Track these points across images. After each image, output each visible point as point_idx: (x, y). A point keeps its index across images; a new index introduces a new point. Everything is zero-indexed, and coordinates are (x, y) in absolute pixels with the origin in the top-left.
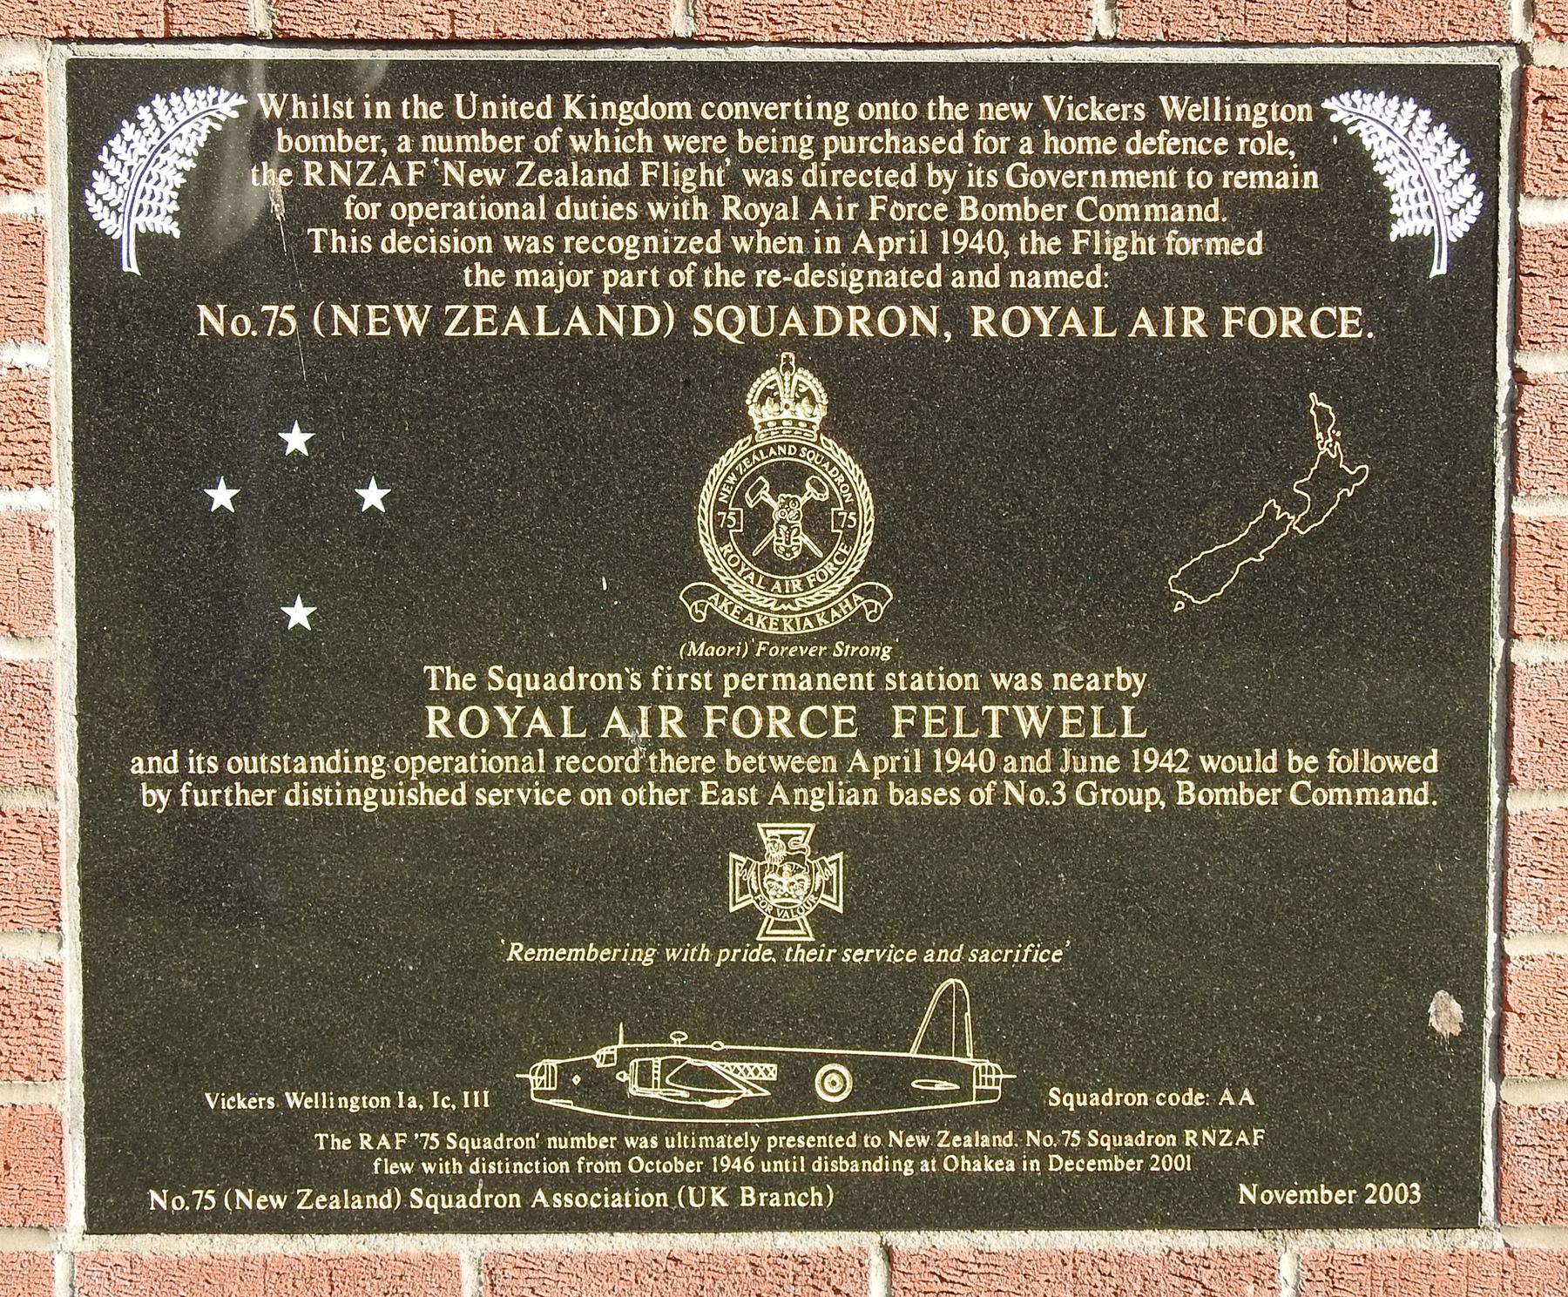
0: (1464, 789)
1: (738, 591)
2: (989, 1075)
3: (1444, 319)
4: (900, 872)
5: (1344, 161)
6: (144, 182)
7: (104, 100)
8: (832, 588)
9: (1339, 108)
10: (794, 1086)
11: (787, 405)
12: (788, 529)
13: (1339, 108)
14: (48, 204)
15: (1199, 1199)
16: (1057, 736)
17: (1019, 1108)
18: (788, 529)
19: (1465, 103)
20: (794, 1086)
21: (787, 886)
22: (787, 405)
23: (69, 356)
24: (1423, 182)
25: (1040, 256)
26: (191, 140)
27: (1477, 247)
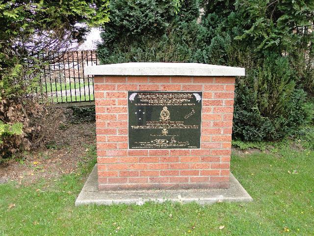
0: (130, 127)
1: (163, 118)
2: (175, 142)
3: (199, 105)
4: (171, 132)
5: (194, 96)
6: (132, 97)
7: (130, 93)
8: (168, 117)
9: (194, 94)
10: (165, 142)
11: (165, 109)
12: (165, 114)
13: (194, 94)
14: (127, 99)
15: (186, 147)
16: (180, 125)
17: (177, 143)
18: (165, 114)
19: (200, 94)
20: (165, 142)
21: (165, 132)
22: (165, 109)
23: (211, 66)
24: (198, 98)
25: (178, 101)
26: (134, 96)
27: (201, 101)
